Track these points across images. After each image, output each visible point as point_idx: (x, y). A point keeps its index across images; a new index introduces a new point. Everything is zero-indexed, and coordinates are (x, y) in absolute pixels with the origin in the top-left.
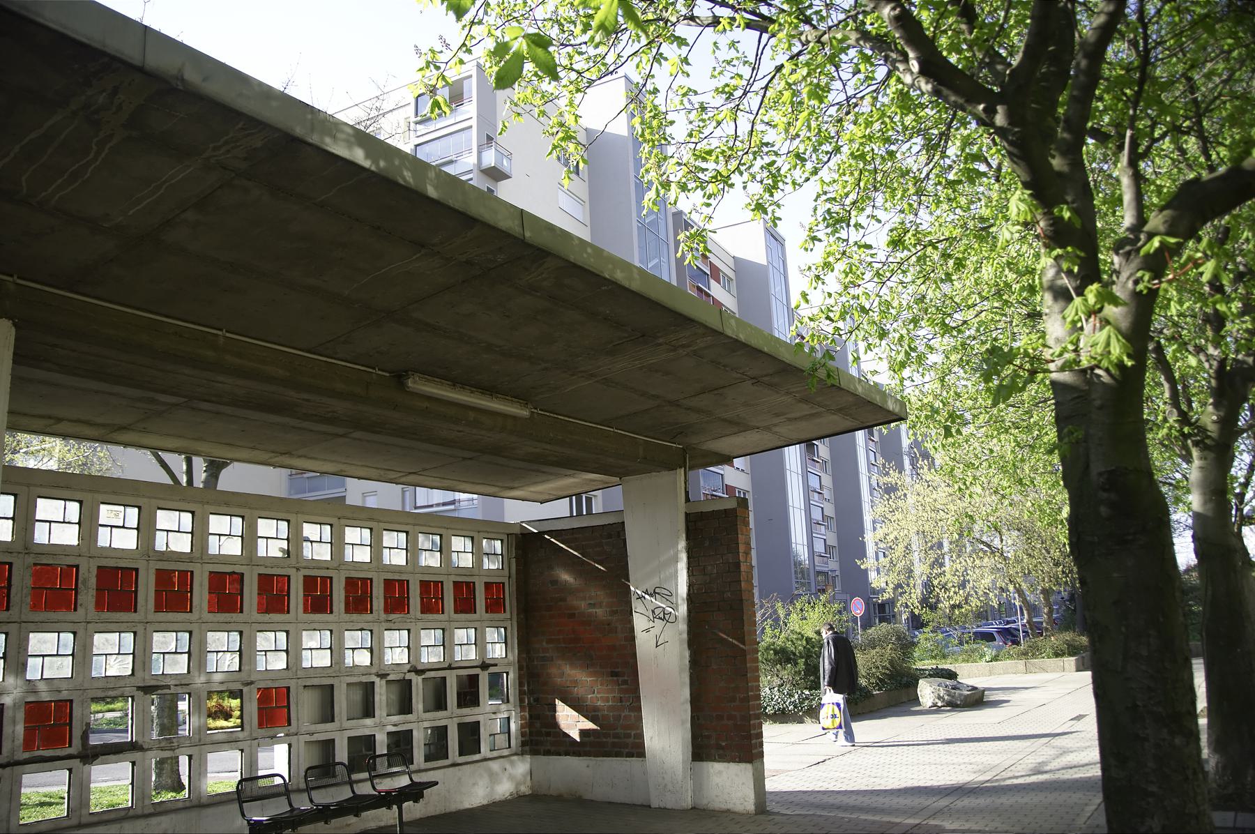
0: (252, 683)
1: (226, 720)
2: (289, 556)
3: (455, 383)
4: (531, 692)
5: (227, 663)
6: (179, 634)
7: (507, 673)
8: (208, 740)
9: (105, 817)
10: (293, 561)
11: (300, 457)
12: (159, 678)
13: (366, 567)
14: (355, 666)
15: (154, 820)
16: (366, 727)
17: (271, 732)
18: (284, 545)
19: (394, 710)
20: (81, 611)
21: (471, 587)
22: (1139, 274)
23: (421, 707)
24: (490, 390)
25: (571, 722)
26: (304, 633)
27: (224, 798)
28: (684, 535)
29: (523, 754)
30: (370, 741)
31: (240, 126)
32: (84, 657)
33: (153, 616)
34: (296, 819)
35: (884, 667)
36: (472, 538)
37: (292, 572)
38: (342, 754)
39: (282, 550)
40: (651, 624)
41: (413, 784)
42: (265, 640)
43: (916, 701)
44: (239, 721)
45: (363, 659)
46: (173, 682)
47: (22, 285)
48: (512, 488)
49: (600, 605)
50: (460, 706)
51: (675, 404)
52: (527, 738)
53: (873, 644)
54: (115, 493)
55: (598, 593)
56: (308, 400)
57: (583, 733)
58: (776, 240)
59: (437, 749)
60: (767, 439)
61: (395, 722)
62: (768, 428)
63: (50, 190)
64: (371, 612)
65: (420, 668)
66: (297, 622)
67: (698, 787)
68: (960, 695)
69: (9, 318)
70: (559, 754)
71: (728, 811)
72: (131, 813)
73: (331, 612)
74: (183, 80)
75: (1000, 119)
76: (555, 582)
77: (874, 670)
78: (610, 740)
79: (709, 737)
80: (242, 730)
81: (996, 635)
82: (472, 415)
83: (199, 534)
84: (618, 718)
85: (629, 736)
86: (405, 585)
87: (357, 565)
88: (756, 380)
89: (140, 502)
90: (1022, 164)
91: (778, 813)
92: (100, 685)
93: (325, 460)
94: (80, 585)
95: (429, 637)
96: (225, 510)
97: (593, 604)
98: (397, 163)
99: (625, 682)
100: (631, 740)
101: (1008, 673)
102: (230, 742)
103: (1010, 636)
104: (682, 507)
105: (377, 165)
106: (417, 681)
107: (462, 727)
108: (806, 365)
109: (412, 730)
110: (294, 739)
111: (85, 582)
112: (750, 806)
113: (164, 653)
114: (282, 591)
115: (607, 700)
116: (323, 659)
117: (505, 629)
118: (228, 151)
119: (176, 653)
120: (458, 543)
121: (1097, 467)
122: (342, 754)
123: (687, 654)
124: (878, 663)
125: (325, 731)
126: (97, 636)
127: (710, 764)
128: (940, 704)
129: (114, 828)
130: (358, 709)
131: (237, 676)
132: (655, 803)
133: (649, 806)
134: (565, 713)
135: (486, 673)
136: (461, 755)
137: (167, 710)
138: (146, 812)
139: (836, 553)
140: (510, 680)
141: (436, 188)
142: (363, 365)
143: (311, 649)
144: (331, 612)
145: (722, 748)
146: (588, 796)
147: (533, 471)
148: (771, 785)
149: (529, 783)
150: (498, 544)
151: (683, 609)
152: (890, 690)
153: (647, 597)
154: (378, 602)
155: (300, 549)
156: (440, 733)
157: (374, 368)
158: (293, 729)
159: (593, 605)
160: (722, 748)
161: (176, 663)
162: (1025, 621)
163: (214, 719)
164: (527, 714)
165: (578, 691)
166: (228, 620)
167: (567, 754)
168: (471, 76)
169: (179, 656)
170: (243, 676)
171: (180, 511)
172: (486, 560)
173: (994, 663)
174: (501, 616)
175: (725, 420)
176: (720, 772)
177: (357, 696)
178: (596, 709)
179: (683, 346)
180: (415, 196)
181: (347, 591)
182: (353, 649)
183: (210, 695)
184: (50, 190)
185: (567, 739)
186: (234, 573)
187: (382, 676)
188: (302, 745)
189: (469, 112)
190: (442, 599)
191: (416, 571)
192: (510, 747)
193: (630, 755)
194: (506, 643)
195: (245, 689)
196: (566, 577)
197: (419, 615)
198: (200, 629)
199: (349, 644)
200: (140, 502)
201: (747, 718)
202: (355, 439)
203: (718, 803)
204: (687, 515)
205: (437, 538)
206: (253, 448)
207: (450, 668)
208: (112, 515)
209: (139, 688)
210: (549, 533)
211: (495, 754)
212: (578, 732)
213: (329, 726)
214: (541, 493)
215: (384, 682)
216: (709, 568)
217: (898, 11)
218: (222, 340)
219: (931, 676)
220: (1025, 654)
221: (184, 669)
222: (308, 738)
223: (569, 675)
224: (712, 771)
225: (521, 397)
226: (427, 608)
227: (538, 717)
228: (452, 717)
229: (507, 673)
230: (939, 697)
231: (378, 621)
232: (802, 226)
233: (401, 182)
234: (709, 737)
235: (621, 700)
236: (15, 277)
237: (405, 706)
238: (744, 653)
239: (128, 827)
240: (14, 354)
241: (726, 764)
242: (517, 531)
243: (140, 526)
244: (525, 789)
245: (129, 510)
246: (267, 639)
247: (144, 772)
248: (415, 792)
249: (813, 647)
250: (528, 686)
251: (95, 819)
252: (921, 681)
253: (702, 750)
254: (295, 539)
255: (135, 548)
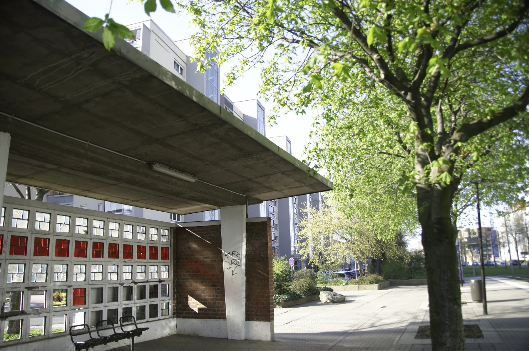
0: (71, 286)
1: (60, 302)
2: (87, 234)
3: (171, 167)
4: (178, 292)
5: (61, 278)
6: (43, 265)
7: (168, 285)
8: (53, 310)
9: (10, 343)
10: (89, 236)
11: (92, 192)
12: (34, 284)
13: (117, 239)
14: (111, 280)
15: (31, 344)
16: (114, 305)
17: (78, 307)
18: (86, 229)
19: (125, 299)
20: (3, 254)
21: (131, 247)
22: (452, 154)
23: (136, 297)
24: (182, 171)
25: (194, 304)
26: (92, 266)
27: (59, 335)
28: (245, 231)
29: (174, 317)
30: (116, 311)
31: (134, 69)
32: (4, 274)
33: (33, 257)
34: (92, 343)
35: (306, 286)
36: (157, 229)
37: (88, 240)
38: (105, 317)
39: (84, 231)
40: (231, 266)
41: (137, 329)
42: (77, 269)
43: (319, 300)
44: (65, 302)
45: (114, 277)
46: (40, 286)
47: (15, 119)
48: (172, 209)
49: (209, 258)
50: (150, 297)
51: (250, 180)
52: (176, 311)
53: (301, 277)
54: (20, 205)
55: (208, 253)
56: (114, 171)
57: (200, 309)
58: (261, 108)
59: (141, 314)
60: (279, 194)
61: (126, 304)
62: (280, 191)
63: (46, 85)
64: (118, 258)
65: (136, 281)
66: (90, 261)
67: (248, 331)
68: (337, 298)
69: (9, 132)
70: (189, 318)
71: (260, 341)
72: (21, 341)
73: (103, 257)
74: (120, 52)
75: (409, 97)
76: (190, 248)
77: (302, 287)
78: (211, 312)
79: (253, 311)
80: (67, 306)
81: (345, 275)
82: (174, 180)
83: (52, 223)
84: (215, 303)
85: (219, 311)
86: (131, 247)
87: (114, 238)
88: (283, 173)
89: (30, 208)
90: (414, 113)
91: (279, 341)
92: (10, 286)
93: (102, 194)
94: (4, 243)
95: (127, 269)
96: (63, 213)
97: (206, 256)
98: (184, 87)
99: (218, 289)
100: (220, 312)
101: (351, 290)
102: (62, 311)
103: (351, 276)
104: (245, 220)
105: (179, 88)
106: (135, 287)
107: (151, 306)
108: (305, 169)
109: (132, 307)
110: (87, 310)
111: (6, 242)
112: (269, 338)
113: (36, 273)
114: (84, 248)
115: (211, 296)
116: (99, 277)
117: (168, 266)
118: (125, 78)
119: (41, 273)
120: (152, 231)
121: (434, 216)
122: (105, 317)
123: (245, 278)
124: (304, 285)
125: (99, 307)
126: (9, 265)
127: (253, 322)
128: (328, 301)
129: (13, 348)
130: (111, 298)
131: (65, 283)
132: (230, 337)
133: (227, 339)
134: (192, 301)
135: (161, 284)
136: (150, 317)
137: (16, 298)
138: (27, 341)
139: (278, 239)
140: (170, 289)
141: (196, 97)
142: (137, 159)
143: (94, 273)
144: (103, 257)
145: (258, 315)
146: (201, 335)
147: (184, 202)
148: (277, 331)
149: (176, 330)
150: (167, 231)
151: (244, 261)
152: (309, 295)
153: (229, 255)
154: (121, 254)
155: (92, 231)
156: (142, 309)
157: (141, 160)
158: (86, 306)
159: (206, 258)
160: (258, 315)
161: (41, 277)
162: (358, 269)
163: (55, 301)
164: (176, 301)
165: (198, 292)
166: (63, 260)
167: (192, 318)
168: (140, 29)
169: (42, 274)
170: (68, 283)
171: (45, 213)
172: (162, 238)
173: (346, 286)
174: (167, 261)
175: (266, 187)
176: (257, 325)
177: (111, 291)
178: (205, 300)
179: (262, 159)
180: (189, 100)
181: (109, 249)
182: (111, 273)
183: (54, 291)
184: (46, 85)
185: (193, 312)
186: (66, 240)
187: (121, 284)
188: (90, 313)
189: (138, 44)
190: (145, 253)
191: (136, 241)
192: (168, 315)
193: (220, 318)
194: (168, 272)
195: (69, 289)
196: (194, 246)
197: (136, 259)
198: (52, 263)
199: (109, 271)
200: (30, 208)
201: (269, 304)
202: (119, 186)
203: (256, 337)
204: (247, 223)
205: (144, 228)
206: (75, 188)
207: (147, 282)
208: (18, 214)
209: (26, 288)
210: (188, 228)
211: (163, 317)
212: (197, 309)
213: (100, 305)
214: (183, 211)
215: (122, 287)
216: (255, 244)
217: (379, 57)
218: (87, 146)
219: (324, 290)
220: (358, 283)
221: (44, 280)
222: (92, 310)
223: (194, 286)
224: (253, 325)
225: (193, 174)
226: (139, 257)
227: (180, 303)
228: (147, 302)
229: (168, 285)
230: (328, 299)
231: (120, 262)
232: (313, 117)
233: (186, 95)
234: (253, 311)
235: (216, 296)
236: (13, 116)
237: (129, 297)
238: (268, 278)
239: (20, 347)
240: (11, 149)
241: (259, 322)
242: (174, 226)
243: (30, 219)
244: (174, 332)
245: (25, 212)
246: (77, 268)
247: (27, 324)
248: (138, 332)
249: (280, 277)
250: (177, 290)
251: (5, 344)
252: (321, 292)
253: (250, 316)
254: (90, 227)
255: (26, 228)
